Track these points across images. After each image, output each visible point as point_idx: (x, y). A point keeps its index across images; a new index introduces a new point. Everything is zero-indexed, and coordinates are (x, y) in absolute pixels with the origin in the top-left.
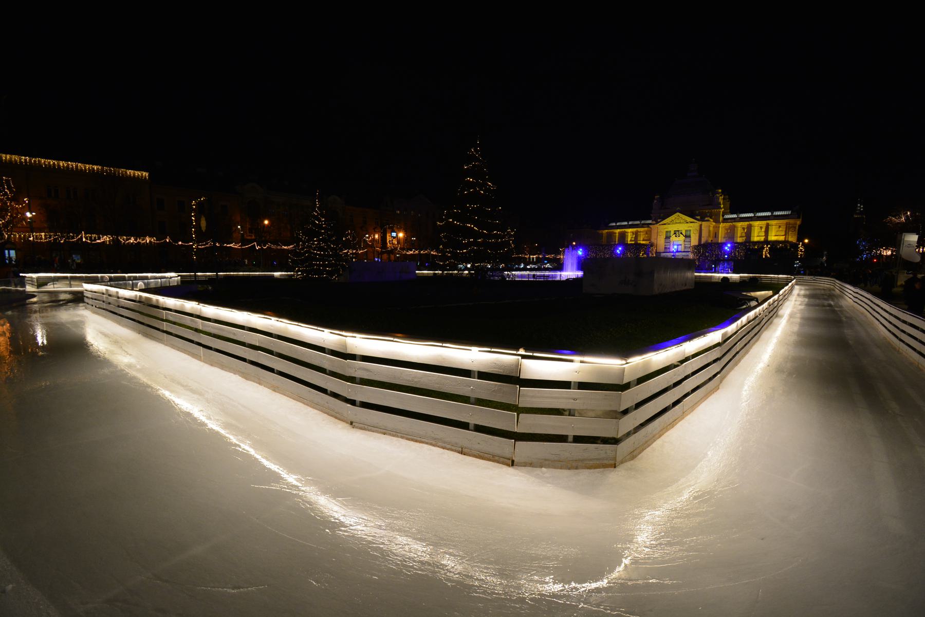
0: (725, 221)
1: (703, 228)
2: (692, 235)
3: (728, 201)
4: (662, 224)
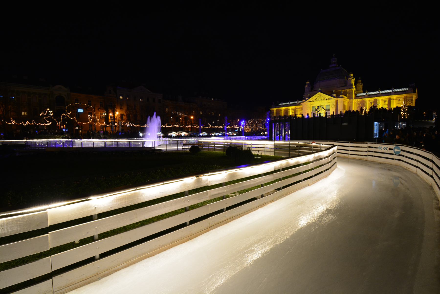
0: (357, 98)
1: (339, 103)
2: (331, 109)
3: (361, 84)
4: (309, 102)
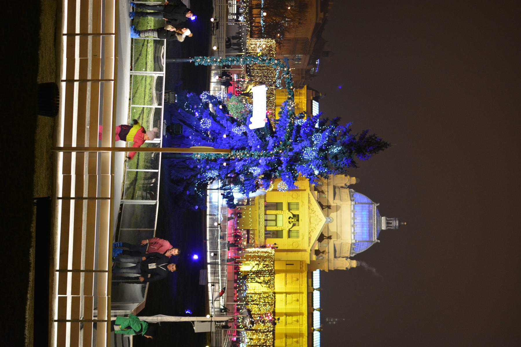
4: (309, 198)
